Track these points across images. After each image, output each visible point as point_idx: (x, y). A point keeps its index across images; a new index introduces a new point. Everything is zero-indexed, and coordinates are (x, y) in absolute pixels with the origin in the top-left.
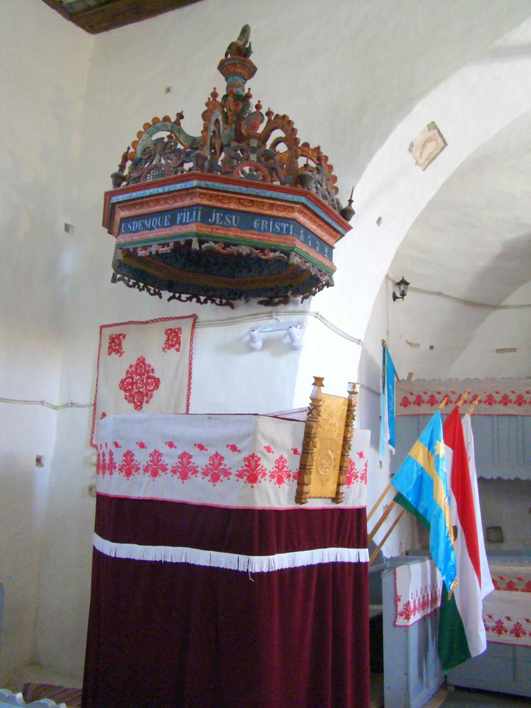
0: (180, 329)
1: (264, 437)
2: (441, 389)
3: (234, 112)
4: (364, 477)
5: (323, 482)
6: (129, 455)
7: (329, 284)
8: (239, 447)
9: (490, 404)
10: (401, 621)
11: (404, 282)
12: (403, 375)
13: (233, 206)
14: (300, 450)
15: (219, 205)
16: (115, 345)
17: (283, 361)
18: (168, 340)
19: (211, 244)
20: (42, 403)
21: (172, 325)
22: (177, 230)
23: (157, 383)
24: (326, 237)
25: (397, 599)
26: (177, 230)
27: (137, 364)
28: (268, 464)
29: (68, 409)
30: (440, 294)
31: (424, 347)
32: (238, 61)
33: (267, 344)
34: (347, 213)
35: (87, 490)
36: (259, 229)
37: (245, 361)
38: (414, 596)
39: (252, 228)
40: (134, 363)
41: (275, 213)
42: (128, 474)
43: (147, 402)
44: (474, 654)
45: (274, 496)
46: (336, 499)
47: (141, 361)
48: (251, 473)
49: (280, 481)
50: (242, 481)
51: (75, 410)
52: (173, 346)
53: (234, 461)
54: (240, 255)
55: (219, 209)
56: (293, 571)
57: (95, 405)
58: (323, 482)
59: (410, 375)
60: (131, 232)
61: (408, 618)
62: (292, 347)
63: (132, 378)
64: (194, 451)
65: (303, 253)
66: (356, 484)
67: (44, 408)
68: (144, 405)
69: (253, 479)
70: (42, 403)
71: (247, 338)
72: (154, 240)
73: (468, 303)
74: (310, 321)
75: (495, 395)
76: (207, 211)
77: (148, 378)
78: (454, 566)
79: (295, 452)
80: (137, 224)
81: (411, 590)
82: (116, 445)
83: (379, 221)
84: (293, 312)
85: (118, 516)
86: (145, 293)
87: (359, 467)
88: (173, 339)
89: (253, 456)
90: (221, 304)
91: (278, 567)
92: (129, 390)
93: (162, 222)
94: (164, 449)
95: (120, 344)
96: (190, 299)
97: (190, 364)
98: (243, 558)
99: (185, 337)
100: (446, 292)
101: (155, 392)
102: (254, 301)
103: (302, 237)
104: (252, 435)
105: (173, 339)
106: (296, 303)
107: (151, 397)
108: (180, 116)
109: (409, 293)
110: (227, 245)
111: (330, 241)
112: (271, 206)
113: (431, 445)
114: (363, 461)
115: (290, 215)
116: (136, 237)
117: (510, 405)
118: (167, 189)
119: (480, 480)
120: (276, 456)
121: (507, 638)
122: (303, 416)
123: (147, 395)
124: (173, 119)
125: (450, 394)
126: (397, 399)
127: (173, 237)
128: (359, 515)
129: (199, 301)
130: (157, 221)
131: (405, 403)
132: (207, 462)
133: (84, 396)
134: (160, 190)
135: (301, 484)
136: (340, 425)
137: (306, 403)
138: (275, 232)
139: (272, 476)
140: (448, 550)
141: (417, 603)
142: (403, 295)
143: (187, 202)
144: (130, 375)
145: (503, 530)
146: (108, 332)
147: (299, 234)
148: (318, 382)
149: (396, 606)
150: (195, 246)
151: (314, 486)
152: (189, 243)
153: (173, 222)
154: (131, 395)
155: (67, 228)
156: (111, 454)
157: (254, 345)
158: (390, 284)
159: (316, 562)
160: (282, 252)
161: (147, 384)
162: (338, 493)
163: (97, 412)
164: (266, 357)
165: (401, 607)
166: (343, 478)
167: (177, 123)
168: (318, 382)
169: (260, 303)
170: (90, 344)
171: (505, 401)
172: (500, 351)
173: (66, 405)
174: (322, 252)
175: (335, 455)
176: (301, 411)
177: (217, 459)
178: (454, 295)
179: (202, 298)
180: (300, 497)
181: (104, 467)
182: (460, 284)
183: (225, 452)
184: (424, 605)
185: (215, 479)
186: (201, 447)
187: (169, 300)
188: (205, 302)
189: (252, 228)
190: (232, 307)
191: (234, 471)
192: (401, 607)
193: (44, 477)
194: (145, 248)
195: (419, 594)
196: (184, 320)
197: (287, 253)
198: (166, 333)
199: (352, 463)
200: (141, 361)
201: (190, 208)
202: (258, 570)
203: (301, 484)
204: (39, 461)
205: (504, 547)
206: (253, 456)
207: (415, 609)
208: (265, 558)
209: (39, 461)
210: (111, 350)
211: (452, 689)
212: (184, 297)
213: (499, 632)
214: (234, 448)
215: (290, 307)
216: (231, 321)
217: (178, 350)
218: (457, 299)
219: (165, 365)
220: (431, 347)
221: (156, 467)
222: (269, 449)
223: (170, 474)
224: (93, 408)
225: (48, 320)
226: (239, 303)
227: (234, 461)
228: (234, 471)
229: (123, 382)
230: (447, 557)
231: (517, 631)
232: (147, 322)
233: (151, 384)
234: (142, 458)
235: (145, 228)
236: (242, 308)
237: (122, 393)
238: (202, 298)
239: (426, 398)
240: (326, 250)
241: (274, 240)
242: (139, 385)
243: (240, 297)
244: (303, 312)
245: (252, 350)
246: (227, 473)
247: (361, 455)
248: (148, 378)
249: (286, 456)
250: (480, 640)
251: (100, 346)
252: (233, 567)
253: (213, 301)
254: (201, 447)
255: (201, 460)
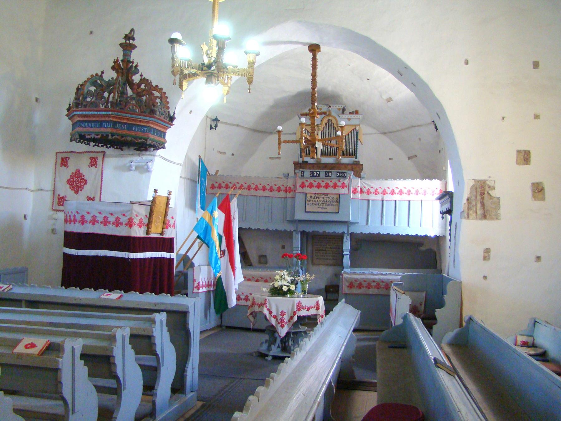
0: (97, 157)
1: (135, 211)
2: (232, 181)
3: (125, 68)
4: (174, 226)
5: (157, 227)
6: (83, 217)
7: (164, 148)
8: (126, 214)
9: (256, 190)
10: (196, 290)
11: (216, 120)
12: (212, 172)
13: (125, 121)
14: (148, 216)
15: (119, 121)
16: (64, 162)
17: (144, 176)
18: (91, 162)
19: (116, 136)
20: (26, 189)
21: (93, 155)
22: (103, 130)
23: (86, 182)
24: (162, 130)
25: (194, 281)
26: (103, 130)
27: (76, 172)
28: (136, 221)
29: (39, 192)
30: (238, 125)
31: (229, 154)
32: (128, 45)
33: (137, 168)
34: (172, 119)
35: (50, 231)
36: (135, 130)
37: (127, 175)
38: (203, 280)
39: (132, 130)
40: (74, 172)
41: (142, 124)
42: (83, 224)
43: (81, 190)
44: (229, 307)
45: (139, 232)
46: (162, 234)
47: (78, 171)
48: (130, 224)
49: (140, 227)
50: (127, 227)
51: (42, 192)
52: (93, 165)
53: (124, 220)
54: (127, 140)
55: (120, 123)
56: (145, 259)
57: (54, 190)
58: (157, 227)
59: (217, 171)
60: (82, 127)
61: (199, 289)
62: (147, 170)
63: (73, 179)
64: (109, 216)
65: (153, 137)
66: (170, 229)
67: (28, 191)
68: (80, 192)
69: (131, 226)
70: (26, 189)
71: (128, 165)
72: (93, 133)
73: (254, 130)
74: (157, 159)
75: (259, 185)
76: (115, 123)
77: (81, 179)
78: (220, 266)
79: (146, 216)
80: (85, 124)
81: (200, 277)
82: (77, 212)
83: (191, 112)
84: (149, 155)
85: (72, 239)
86: (83, 144)
87: (172, 222)
88: (93, 162)
89: (131, 218)
90: (117, 149)
91: (139, 257)
92: (72, 185)
93: (96, 125)
94: (97, 215)
95: (67, 162)
96: (103, 146)
97: (102, 174)
98: (127, 253)
99: (99, 161)
100: (241, 125)
101: (85, 186)
102: (132, 148)
103: (152, 133)
104: (131, 210)
105: (93, 162)
106: (150, 151)
107: (83, 188)
108: (102, 72)
109: (219, 125)
110: (122, 137)
111: (164, 131)
112: (140, 121)
113: (212, 213)
114: (173, 220)
115: (148, 125)
116: (85, 130)
117: (266, 191)
118: (99, 113)
119: (240, 229)
120: (139, 218)
121: (243, 302)
122: (150, 204)
123: (81, 187)
124: (100, 74)
125: (236, 184)
126: (207, 185)
127: (101, 132)
128: (171, 240)
129: (107, 147)
130: (94, 124)
131: (213, 187)
132: (114, 220)
133: (48, 185)
134: (96, 113)
135: (148, 228)
136: (164, 207)
137: (151, 199)
138: (141, 131)
139: (138, 225)
140: (217, 260)
141: (204, 284)
142: (216, 126)
143: (107, 119)
144: (72, 177)
145: (268, 257)
146: (60, 156)
147: (151, 131)
148: (156, 191)
149: (194, 284)
150: (110, 137)
151: (153, 229)
152: (108, 135)
153: (101, 126)
154: (73, 187)
155: (37, 100)
156: (74, 216)
157: (132, 169)
158: (209, 120)
159: (154, 256)
160: (144, 139)
161: (81, 182)
162: (162, 232)
163: (55, 194)
164: (137, 174)
165: (196, 284)
166: (165, 226)
167: (101, 76)
168: (156, 191)
169: (135, 149)
170: (50, 161)
171: (264, 189)
172: (271, 158)
173: (38, 190)
174: (161, 136)
175: (161, 218)
176: (149, 201)
177: (118, 219)
178: (246, 126)
179: (108, 146)
180: (148, 232)
181: (70, 221)
182: (250, 121)
183: (121, 216)
184: (209, 285)
185: (117, 226)
186: (112, 214)
187: (94, 146)
188: (110, 147)
189: (132, 130)
190: (122, 150)
191: (124, 223)
192: (196, 284)
193: (27, 224)
194: (89, 135)
195: (206, 280)
196: (99, 154)
197: (146, 140)
198: (90, 158)
199: (169, 221)
200: (78, 171)
201: (108, 122)
202: (132, 258)
203: (148, 228)
204: (25, 217)
205: (268, 265)
206: (131, 218)
207: (203, 286)
208: (135, 254)
209: (25, 217)
210: (62, 165)
211: (224, 328)
212: (100, 145)
213: (246, 301)
214: (124, 215)
215: (148, 153)
216: (122, 156)
217: (96, 167)
218: (248, 129)
219: (89, 173)
220: (233, 154)
221: (94, 221)
222: (137, 216)
223: (100, 224)
224: (52, 192)
225: (22, 142)
226: (124, 148)
227: (124, 220)
228: (124, 223)
229: (68, 180)
230: (216, 263)
231: (247, 299)
232: (81, 153)
233: (83, 182)
234: (88, 218)
235: (89, 126)
236: (126, 151)
237: (68, 186)
238: (108, 146)
239: (224, 185)
240: (163, 135)
241: (141, 135)
242: (77, 182)
243: (125, 146)
244: (154, 155)
245: (131, 170)
246: (97, 222)
247: (172, 218)
248: (81, 179)
249: (143, 218)
250: (233, 301)
251: (56, 162)
252: (124, 257)
253: (113, 147)
254: (112, 214)
255: (112, 219)
